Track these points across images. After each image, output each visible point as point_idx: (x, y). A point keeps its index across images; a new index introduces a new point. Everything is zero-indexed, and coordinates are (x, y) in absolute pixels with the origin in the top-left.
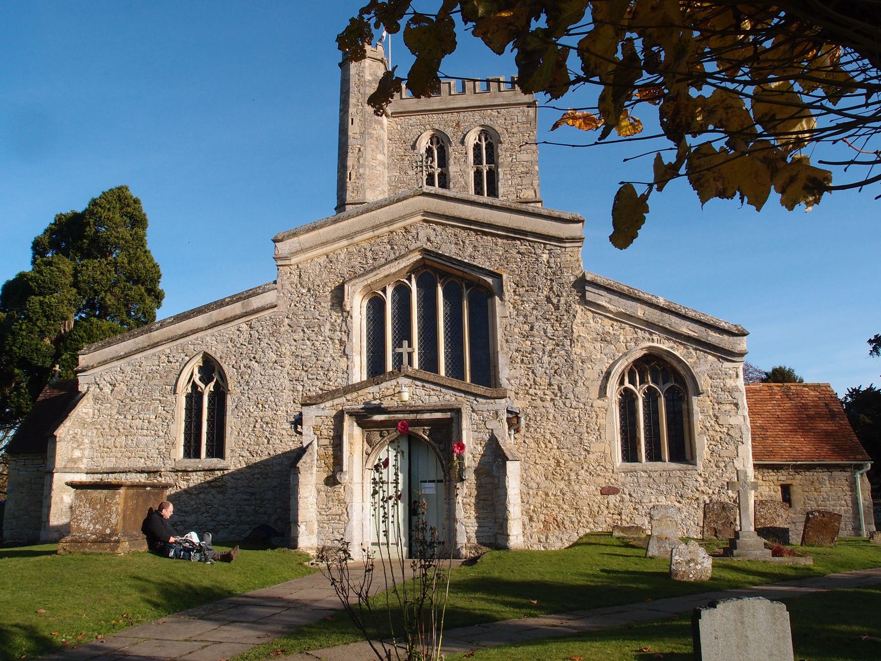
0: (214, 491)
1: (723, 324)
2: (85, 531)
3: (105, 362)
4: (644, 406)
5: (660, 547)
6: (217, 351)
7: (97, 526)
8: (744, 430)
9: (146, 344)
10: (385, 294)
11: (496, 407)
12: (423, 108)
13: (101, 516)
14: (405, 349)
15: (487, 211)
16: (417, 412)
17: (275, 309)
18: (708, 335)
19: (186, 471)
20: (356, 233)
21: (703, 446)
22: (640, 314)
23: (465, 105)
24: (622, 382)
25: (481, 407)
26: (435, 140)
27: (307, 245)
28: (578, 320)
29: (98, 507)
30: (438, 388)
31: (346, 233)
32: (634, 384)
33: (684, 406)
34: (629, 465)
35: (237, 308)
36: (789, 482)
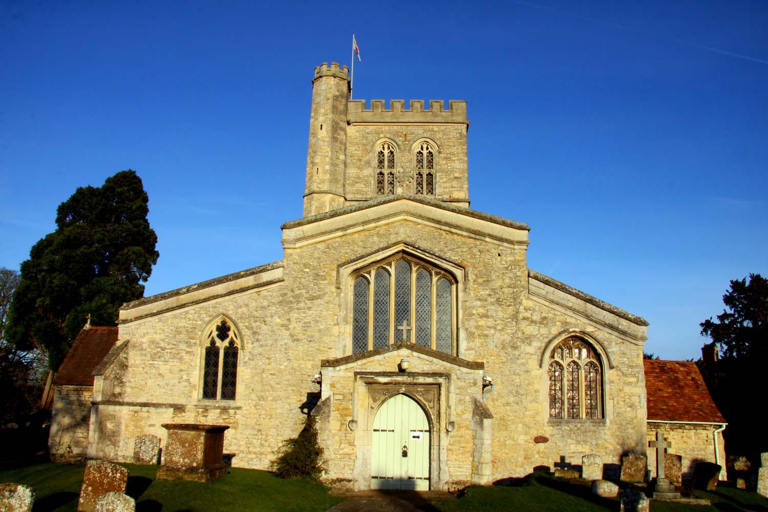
1: (630, 316)
2: (176, 463)
7: (186, 460)
9: (175, 305)
10: (370, 276)
13: (189, 452)
14: (404, 327)
17: (282, 283)
20: (349, 227)
24: (553, 357)
26: (386, 146)
27: (310, 234)
29: (187, 445)
31: (341, 226)
35: (250, 281)
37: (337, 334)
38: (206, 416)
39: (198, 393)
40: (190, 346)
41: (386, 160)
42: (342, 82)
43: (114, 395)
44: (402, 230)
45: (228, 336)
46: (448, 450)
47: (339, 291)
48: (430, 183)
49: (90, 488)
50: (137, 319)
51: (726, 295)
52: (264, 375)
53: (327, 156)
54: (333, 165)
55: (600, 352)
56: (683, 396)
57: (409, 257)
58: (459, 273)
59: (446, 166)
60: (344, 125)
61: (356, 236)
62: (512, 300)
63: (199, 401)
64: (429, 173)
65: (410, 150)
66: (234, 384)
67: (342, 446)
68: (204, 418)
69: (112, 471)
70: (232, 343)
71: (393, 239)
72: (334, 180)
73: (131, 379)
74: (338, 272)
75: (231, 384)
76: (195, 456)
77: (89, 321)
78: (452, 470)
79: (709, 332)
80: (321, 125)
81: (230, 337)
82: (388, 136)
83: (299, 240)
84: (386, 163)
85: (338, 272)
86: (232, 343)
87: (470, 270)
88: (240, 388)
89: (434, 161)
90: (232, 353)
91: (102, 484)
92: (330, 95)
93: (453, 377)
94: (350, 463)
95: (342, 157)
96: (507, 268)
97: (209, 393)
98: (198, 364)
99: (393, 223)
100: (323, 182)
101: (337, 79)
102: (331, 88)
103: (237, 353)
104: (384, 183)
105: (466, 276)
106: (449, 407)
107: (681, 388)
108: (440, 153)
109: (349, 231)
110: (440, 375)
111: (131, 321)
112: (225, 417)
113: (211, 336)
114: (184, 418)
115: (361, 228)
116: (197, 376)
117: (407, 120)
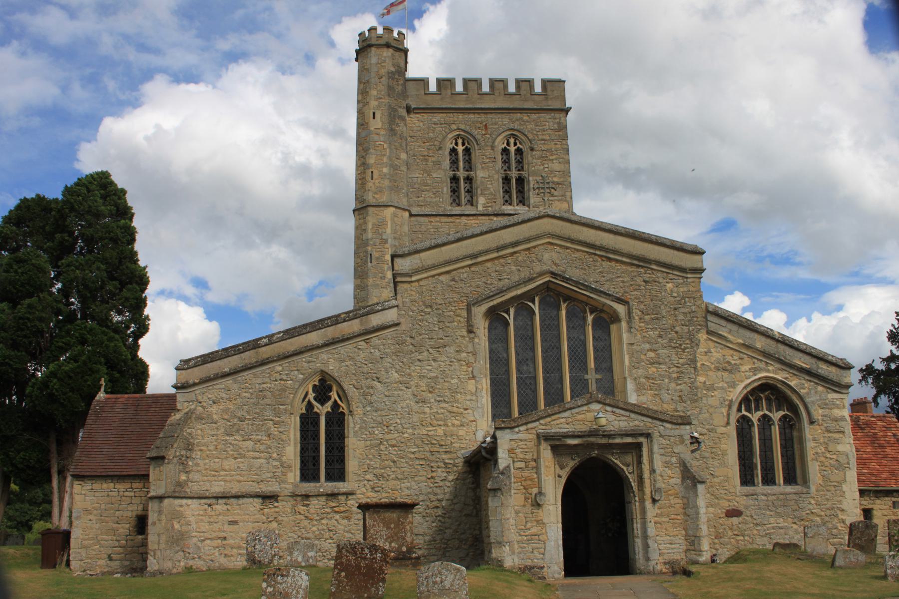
0: (337, 517)
3: (207, 380)
4: (759, 434)
5: (845, 558)
6: (332, 368)
7: (393, 545)
8: (850, 456)
10: (509, 315)
11: (683, 433)
12: (449, 106)
13: (396, 535)
15: (612, 236)
16: (610, 436)
18: (818, 367)
19: (307, 496)
21: (814, 469)
22: (759, 346)
23: (492, 106)
24: (739, 410)
25: (668, 432)
28: (702, 349)
29: (392, 526)
30: (627, 414)
32: (770, 411)
33: (795, 434)
34: (748, 489)
36: (870, 506)
37: (474, 390)
38: (307, 505)
39: (294, 475)
40: (278, 414)
41: (463, 156)
42: (397, 54)
43: (179, 484)
44: (546, 256)
45: (329, 398)
46: (655, 523)
47: (472, 335)
48: (521, 191)
49: (343, 574)
50: (203, 381)
51: (891, 331)
52: (382, 447)
53: (384, 155)
54: (394, 167)
55: (798, 402)
56: (885, 457)
57: (553, 293)
58: (620, 309)
59: (542, 167)
60: (403, 112)
61: (489, 264)
62: (688, 341)
63: (296, 486)
64: (520, 177)
65: (493, 148)
66: (342, 460)
67: (529, 525)
68: (305, 508)
69: (371, 552)
70: (336, 405)
71: (538, 268)
72: (395, 189)
73: (199, 461)
74: (469, 311)
75: (337, 461)
76: (404, 539)
77: (103, 389)
78: (661, 547)
79: (870, 381)
80: (374, 114)
81: (333, 400)
82: (463, 127)
83: (417, 271)
84: (461, 164)
85: (469, 311)
86: (336, 405)
87: (634, 304)
88: (352, 465)
89: (525, 161)
90: (337, 420)
91: (358, 567)
92: (383, 72)
93: (656, 435)
94: (540, 546)
95: (403, 156)
96: (679, 302)
97: (308, 473)
98: (292, 437)
99: (534, 247)
100: (380, 190)
101: (391, 50)
102: (385, 61)
103: (344, 420)
104: (462, 187)
105: (629, 313)
106: (653, 471)
107: (881, 446)
108: (532, 149)
109: (480, 259)
110: (641, 435)
111: (195, 384)
112: (334, 504)
113: (307, 400)
114: (277, 510)
115: (495, 255)
116: (292, 452)
117: (487, 106)
